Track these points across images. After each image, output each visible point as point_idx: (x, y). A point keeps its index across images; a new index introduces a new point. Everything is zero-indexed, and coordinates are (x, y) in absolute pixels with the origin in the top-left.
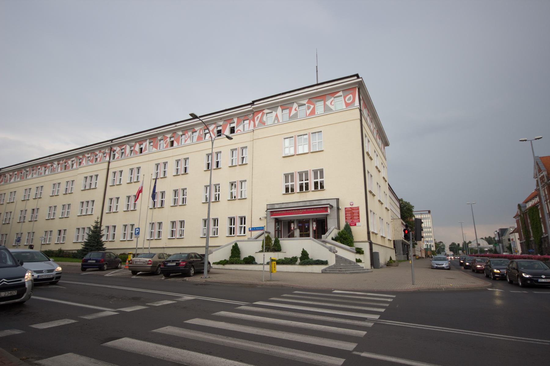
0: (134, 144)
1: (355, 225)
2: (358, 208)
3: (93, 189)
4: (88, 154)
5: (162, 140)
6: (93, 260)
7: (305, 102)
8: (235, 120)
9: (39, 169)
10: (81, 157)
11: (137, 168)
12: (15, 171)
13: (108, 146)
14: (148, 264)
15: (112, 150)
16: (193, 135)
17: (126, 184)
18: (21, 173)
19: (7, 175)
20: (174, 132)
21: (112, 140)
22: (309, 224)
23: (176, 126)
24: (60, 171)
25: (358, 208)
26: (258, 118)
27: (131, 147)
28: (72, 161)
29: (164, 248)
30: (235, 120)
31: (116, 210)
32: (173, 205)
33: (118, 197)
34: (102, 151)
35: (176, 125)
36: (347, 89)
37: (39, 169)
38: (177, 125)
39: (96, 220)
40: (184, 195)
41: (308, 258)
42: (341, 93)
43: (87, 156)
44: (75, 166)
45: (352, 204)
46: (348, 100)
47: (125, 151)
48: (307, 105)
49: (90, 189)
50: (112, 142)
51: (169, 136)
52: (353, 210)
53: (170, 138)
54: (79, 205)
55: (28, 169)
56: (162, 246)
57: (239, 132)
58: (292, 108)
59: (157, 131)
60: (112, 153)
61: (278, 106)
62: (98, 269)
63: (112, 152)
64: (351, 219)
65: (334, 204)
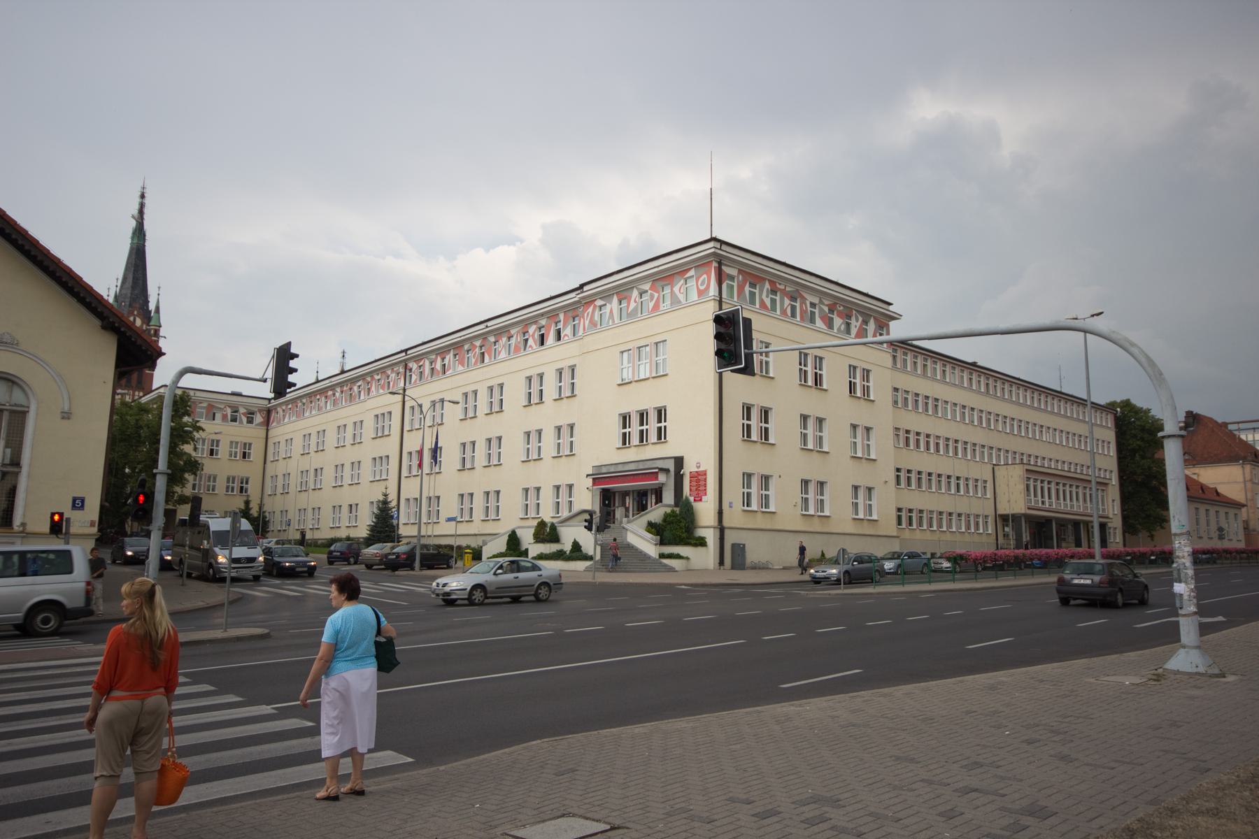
0: (434, 357)
1: (701, 500)
2: (705, 473)
3: (386, 436)
4: (378, 374)
5: (470, 350)
6: (338, 552)
7: (646, 287)
8: (562, 316)
9: (319, 399)
10: (369, 379)
11: (538, 375)
12: (690, 269)
13: (401, 362)
14: (376, 557)
15: (408, 368)
16: (642, 300)
17: (483, 415)
18: (297, 406)
19: (279, 409)
20: (484, 336)
21: (406, 351)
22: (647, 498)
23: (487, 327)
24: (696, 298)
25: (705, 473)
26: (588, 314)
27: (431, 363)
28: (359, 386)
29: (476, 535)
30: (562, 316)
31: (499, 461)
32: (556, 455)
33: (571, 422)
34: (395, 369)
35: (485, 324)
36: (700, 264)
37: (319, 399)
38: (489, 324)
39: (384, 491)
40: (625, 427)
41: (581, 551)
42: (692, 273)
43: (377, 377)
44: (362, 397)
45: (698, 465)
46: (701, 285)
47: (424, 370)
48: (649, 292)
49: (382, 437)
50: (406, 355)
51: (478, 343)
52: (699, 475)
53: (481, 347)
54: (521, 438)
55: (304, 401)
56: (473, 533)
57: (566, 338)
58: (631, 297)
59: (460, 337)
60: (408, 374)
61: (613, 294)
62: (383, 567)
63: (408, 371)
64: (696, 490)
65: (670, 465)
